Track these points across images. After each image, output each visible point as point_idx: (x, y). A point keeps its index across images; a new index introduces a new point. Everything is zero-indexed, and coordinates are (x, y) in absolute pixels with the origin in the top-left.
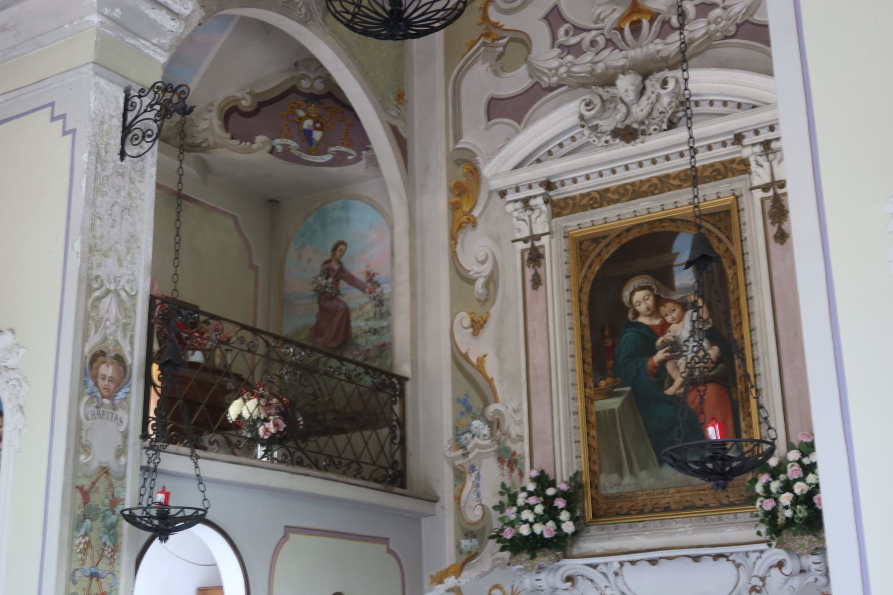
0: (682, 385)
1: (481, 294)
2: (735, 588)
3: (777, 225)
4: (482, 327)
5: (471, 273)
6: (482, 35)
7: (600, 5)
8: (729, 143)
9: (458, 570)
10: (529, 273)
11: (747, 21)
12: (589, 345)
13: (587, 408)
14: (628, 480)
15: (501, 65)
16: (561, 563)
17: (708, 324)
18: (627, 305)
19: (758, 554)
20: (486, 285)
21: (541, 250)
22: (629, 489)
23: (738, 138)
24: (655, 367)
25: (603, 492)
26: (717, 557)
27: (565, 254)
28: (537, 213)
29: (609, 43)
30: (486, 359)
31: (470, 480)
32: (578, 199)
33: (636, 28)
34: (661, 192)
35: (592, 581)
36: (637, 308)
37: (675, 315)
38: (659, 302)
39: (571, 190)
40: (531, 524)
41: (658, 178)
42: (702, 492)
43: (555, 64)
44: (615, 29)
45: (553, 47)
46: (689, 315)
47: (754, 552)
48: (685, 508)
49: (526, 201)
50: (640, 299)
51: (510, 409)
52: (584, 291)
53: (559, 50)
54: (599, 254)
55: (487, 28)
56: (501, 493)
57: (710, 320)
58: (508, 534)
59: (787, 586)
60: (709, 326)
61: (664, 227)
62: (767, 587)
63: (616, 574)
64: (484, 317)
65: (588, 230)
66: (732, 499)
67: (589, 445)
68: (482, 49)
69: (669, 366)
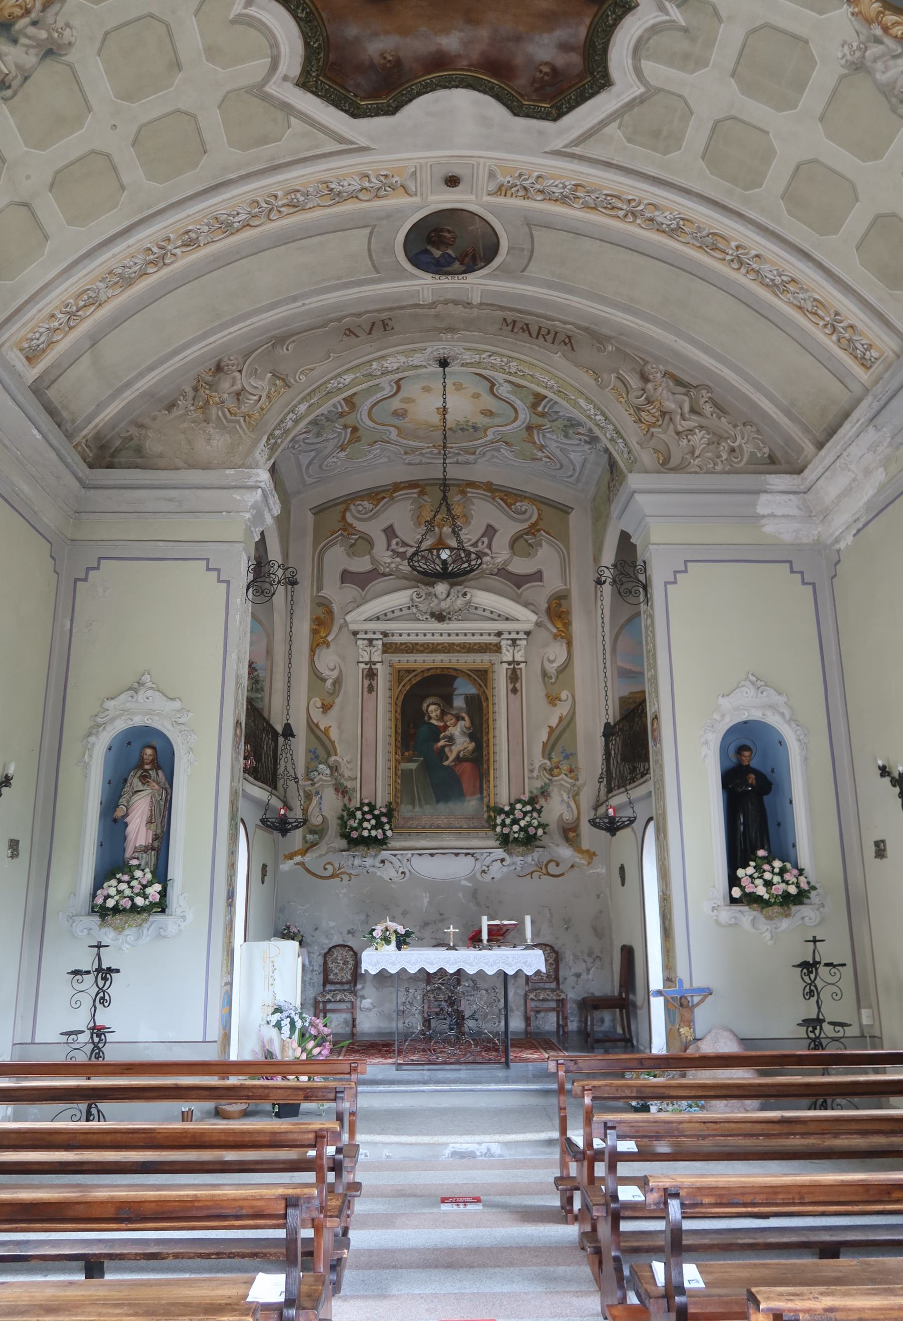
0: (453, 761)
9: (304, 853)
10: (367, 683)
12: (400, 731)
14: (417, 809)
20: (334, 684)
21: (375, 671)
23: (499, 634)
26: (467, 854)
28: (375, 649)
31: (315, 800)
37: (452, 722)
38: (443, 713)
39: (396, 639)
43: (389, 560)
46: (461, 723)
49: (370, 641)
50: (433, 710)
65: (405, 665)
69: (447, 749)
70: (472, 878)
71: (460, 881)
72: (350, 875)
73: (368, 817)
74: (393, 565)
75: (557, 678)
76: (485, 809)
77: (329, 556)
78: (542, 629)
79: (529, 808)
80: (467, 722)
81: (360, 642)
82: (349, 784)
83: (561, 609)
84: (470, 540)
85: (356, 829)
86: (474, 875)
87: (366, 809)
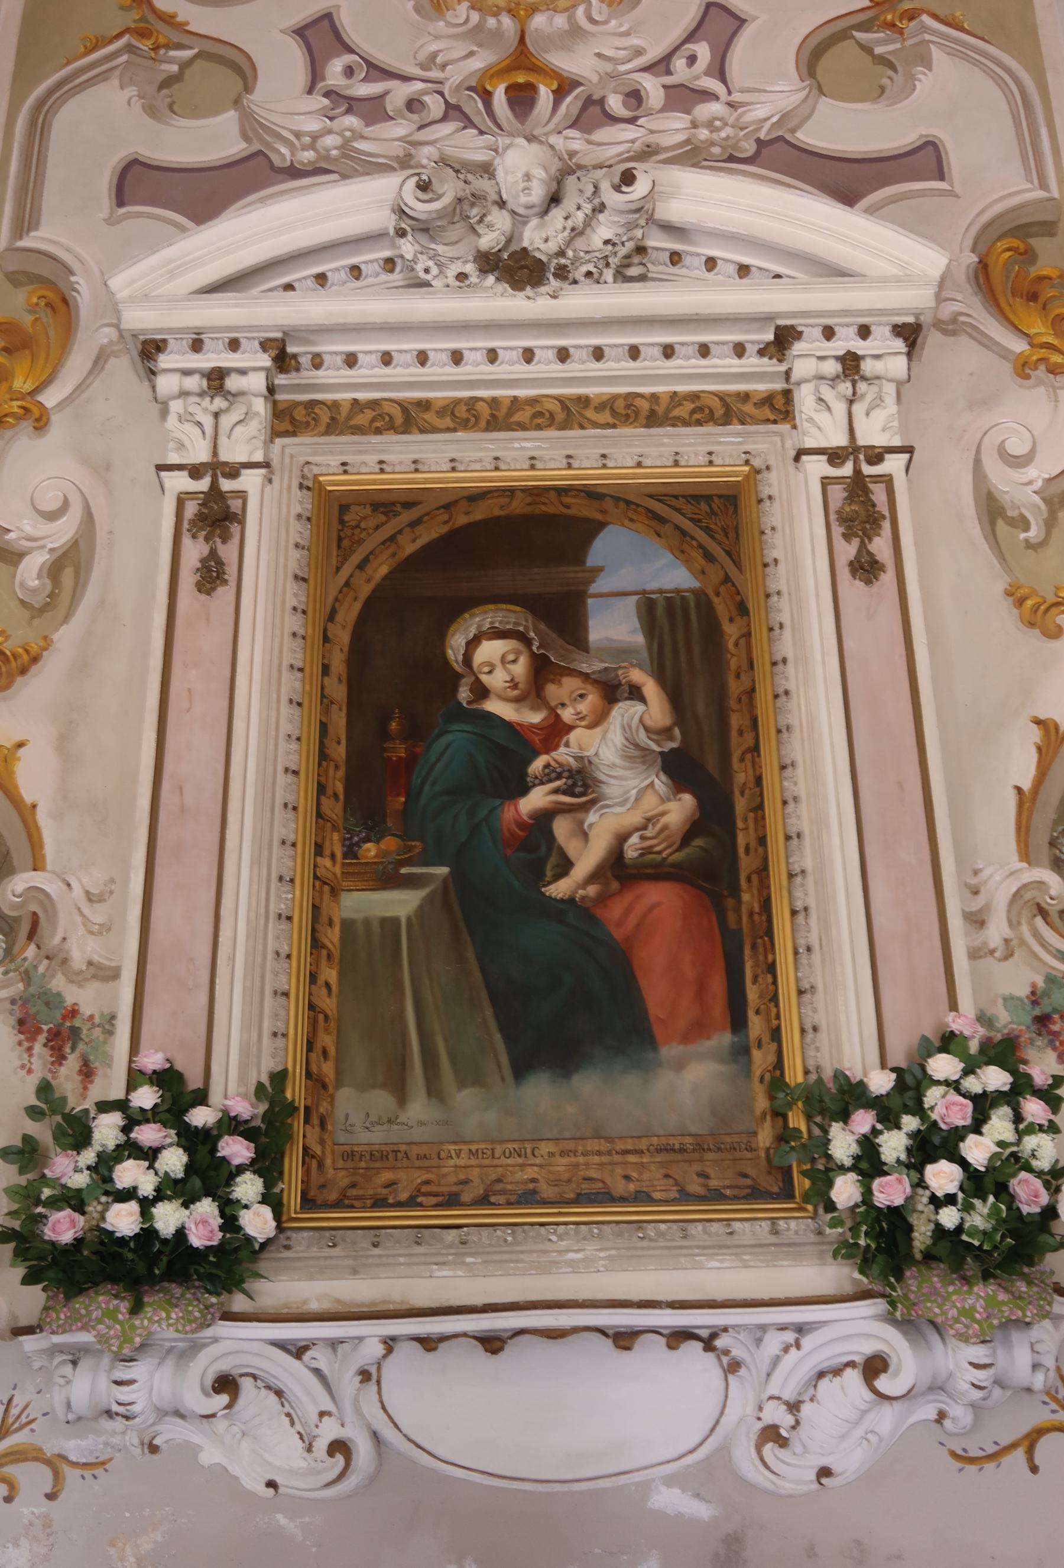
0: (593, 877)
1: (34, 591)
2: (713, 1430)
3: (856, 542)
4: (23, 671)
5: (12, 536)
6: (127, 30)
7: (437, 37)
8: (751, 349)
10: (194, 552)
11: (781, 139)
12: (340, 752)
13: (316, 909)
15: (168, 97)
16: (209, 1332)
17: (671, 738)
18: (458, 667)
19: (790, 1337)
20: (54, 571)
21: (235, 505)
22: (418, 1134)
24: (521, 825)
25: (342, 1138)
26: (678, 1337)
27: (295, 525)
29: (452, 111)
30: (21, 752)
32: (344, 411)
33: (522, 98)
34: (563, 427)
35: (279, 1393)
36: (484, 678)
37: (583, 707)
38: (543, 671)
39: (334, 383)
40: (146, 1205)
41: (560, 400)
42: (631, 1158)
43: (313, 125)
44: (470, 88)
45: (310, 92)
46: (626, 712)
47: (783, 1328)
48: (580, 1199)
49: (216, 379)
50: (493, 659)
51: (78, 891)
52: (339, 617)
53: (326, 102)
54: (392, 539)
55: (143, 19)
56: (34, 1113)
57: (677, 731)
58: (63, 1228)
59: (860, 1431)
60: (674, 745)
61: (568, 507)
62: (803, 1431)
63: (365, 1375)
64: (34, 649)
66: (714, 1183)
67: (312, 1007)
68: (125, 58)
69: (561, 827)
70: (709, 1472)
71: (646, 1487)
72: (56, 1463)
73: (148, 1135)
74: (330, 141)
75: (1050, 523)
76: (762, 1103)
77: (72, 119)
78: (963, 339)
79: (995, 1078)
80: (655, 707)
81: (167, 384)
82: (86, 999)
83: (1034, 271)
84: (639, 52)
85: (75, 1201)
86: (724, 1450)
87: (146, 1097)
